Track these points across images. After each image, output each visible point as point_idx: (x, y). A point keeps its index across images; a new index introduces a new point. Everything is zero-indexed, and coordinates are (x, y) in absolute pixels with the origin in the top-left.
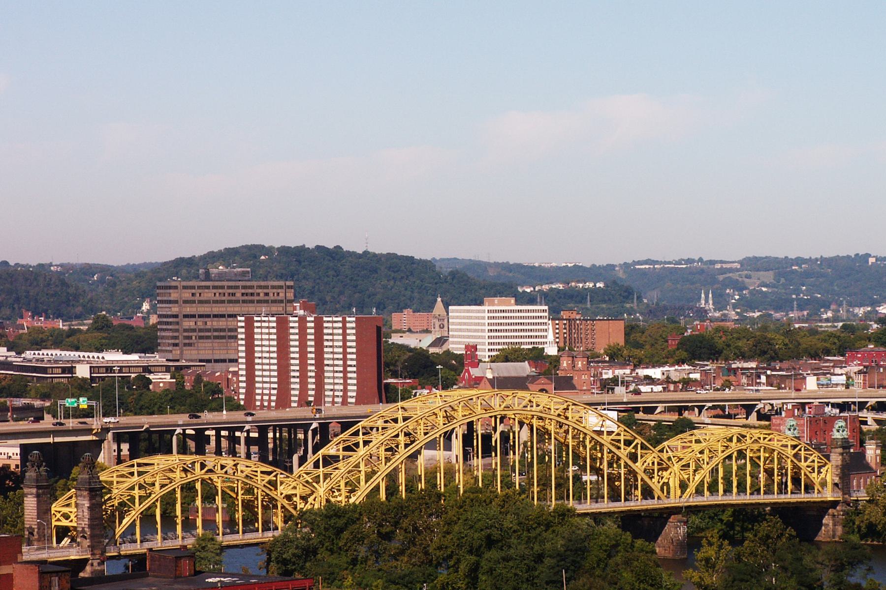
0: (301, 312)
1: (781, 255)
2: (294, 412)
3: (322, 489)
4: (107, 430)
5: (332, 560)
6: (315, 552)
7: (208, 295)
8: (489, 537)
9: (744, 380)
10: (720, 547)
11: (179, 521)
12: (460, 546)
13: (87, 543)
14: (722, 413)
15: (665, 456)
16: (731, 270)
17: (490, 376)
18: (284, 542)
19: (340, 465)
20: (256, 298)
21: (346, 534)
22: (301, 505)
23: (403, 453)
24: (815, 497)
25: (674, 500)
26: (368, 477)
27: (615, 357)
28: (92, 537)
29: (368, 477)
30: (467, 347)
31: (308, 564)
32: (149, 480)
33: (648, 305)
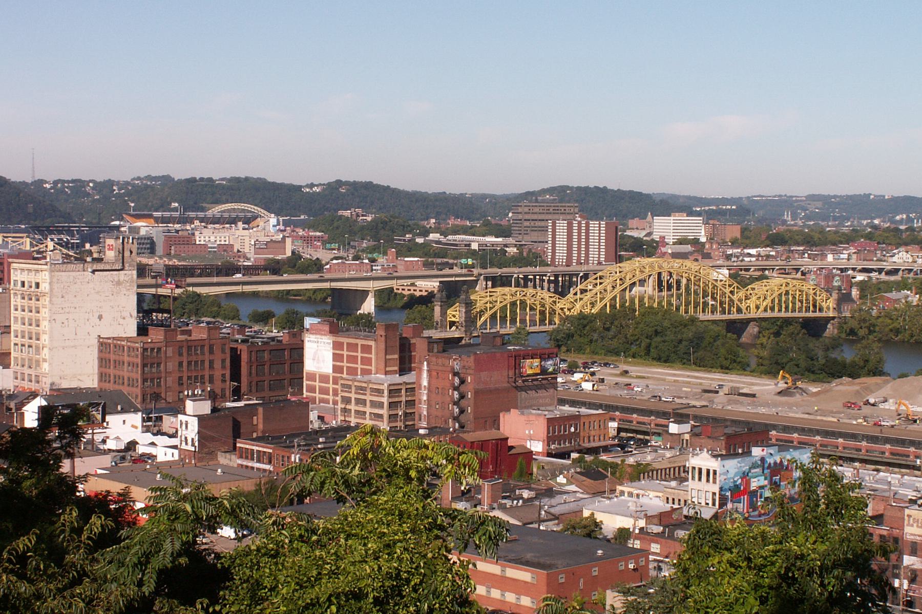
0: (579, 219)
1: (826, 194)
2: (574, 267)
3: (578, 306)
4: (481, 275)
5: (581, 340)
6: (573, 336)
7: (536, 210)
8: (656, 331)
9: (797, 256)
10: (769, 338)
11: (508, 319)
12: (642, 335)
13: (463, 329)
14: (783, 272)
15: (748, 293)
16: (801, 201)
17: (670, 251)
18: (557, 331)
19: (588, 293)
20: (559, 212)
21: (588, 328)
22: (567, 313)
23: (619, 289)
24: (823, 314)
25: (752, 315)
26: (601, 299)
27: (735, 243)
28: (466, 326)
29: (601, 299)
30: (660, 238)
31: (569, 342)
32: (494, 299)
33: (757, 217)
